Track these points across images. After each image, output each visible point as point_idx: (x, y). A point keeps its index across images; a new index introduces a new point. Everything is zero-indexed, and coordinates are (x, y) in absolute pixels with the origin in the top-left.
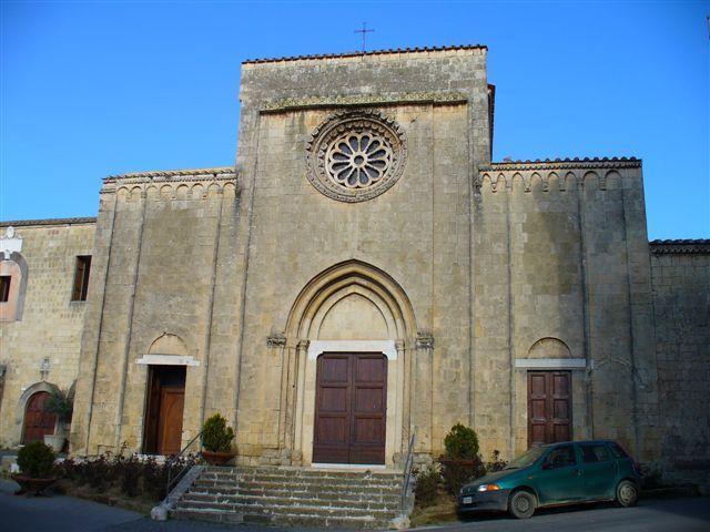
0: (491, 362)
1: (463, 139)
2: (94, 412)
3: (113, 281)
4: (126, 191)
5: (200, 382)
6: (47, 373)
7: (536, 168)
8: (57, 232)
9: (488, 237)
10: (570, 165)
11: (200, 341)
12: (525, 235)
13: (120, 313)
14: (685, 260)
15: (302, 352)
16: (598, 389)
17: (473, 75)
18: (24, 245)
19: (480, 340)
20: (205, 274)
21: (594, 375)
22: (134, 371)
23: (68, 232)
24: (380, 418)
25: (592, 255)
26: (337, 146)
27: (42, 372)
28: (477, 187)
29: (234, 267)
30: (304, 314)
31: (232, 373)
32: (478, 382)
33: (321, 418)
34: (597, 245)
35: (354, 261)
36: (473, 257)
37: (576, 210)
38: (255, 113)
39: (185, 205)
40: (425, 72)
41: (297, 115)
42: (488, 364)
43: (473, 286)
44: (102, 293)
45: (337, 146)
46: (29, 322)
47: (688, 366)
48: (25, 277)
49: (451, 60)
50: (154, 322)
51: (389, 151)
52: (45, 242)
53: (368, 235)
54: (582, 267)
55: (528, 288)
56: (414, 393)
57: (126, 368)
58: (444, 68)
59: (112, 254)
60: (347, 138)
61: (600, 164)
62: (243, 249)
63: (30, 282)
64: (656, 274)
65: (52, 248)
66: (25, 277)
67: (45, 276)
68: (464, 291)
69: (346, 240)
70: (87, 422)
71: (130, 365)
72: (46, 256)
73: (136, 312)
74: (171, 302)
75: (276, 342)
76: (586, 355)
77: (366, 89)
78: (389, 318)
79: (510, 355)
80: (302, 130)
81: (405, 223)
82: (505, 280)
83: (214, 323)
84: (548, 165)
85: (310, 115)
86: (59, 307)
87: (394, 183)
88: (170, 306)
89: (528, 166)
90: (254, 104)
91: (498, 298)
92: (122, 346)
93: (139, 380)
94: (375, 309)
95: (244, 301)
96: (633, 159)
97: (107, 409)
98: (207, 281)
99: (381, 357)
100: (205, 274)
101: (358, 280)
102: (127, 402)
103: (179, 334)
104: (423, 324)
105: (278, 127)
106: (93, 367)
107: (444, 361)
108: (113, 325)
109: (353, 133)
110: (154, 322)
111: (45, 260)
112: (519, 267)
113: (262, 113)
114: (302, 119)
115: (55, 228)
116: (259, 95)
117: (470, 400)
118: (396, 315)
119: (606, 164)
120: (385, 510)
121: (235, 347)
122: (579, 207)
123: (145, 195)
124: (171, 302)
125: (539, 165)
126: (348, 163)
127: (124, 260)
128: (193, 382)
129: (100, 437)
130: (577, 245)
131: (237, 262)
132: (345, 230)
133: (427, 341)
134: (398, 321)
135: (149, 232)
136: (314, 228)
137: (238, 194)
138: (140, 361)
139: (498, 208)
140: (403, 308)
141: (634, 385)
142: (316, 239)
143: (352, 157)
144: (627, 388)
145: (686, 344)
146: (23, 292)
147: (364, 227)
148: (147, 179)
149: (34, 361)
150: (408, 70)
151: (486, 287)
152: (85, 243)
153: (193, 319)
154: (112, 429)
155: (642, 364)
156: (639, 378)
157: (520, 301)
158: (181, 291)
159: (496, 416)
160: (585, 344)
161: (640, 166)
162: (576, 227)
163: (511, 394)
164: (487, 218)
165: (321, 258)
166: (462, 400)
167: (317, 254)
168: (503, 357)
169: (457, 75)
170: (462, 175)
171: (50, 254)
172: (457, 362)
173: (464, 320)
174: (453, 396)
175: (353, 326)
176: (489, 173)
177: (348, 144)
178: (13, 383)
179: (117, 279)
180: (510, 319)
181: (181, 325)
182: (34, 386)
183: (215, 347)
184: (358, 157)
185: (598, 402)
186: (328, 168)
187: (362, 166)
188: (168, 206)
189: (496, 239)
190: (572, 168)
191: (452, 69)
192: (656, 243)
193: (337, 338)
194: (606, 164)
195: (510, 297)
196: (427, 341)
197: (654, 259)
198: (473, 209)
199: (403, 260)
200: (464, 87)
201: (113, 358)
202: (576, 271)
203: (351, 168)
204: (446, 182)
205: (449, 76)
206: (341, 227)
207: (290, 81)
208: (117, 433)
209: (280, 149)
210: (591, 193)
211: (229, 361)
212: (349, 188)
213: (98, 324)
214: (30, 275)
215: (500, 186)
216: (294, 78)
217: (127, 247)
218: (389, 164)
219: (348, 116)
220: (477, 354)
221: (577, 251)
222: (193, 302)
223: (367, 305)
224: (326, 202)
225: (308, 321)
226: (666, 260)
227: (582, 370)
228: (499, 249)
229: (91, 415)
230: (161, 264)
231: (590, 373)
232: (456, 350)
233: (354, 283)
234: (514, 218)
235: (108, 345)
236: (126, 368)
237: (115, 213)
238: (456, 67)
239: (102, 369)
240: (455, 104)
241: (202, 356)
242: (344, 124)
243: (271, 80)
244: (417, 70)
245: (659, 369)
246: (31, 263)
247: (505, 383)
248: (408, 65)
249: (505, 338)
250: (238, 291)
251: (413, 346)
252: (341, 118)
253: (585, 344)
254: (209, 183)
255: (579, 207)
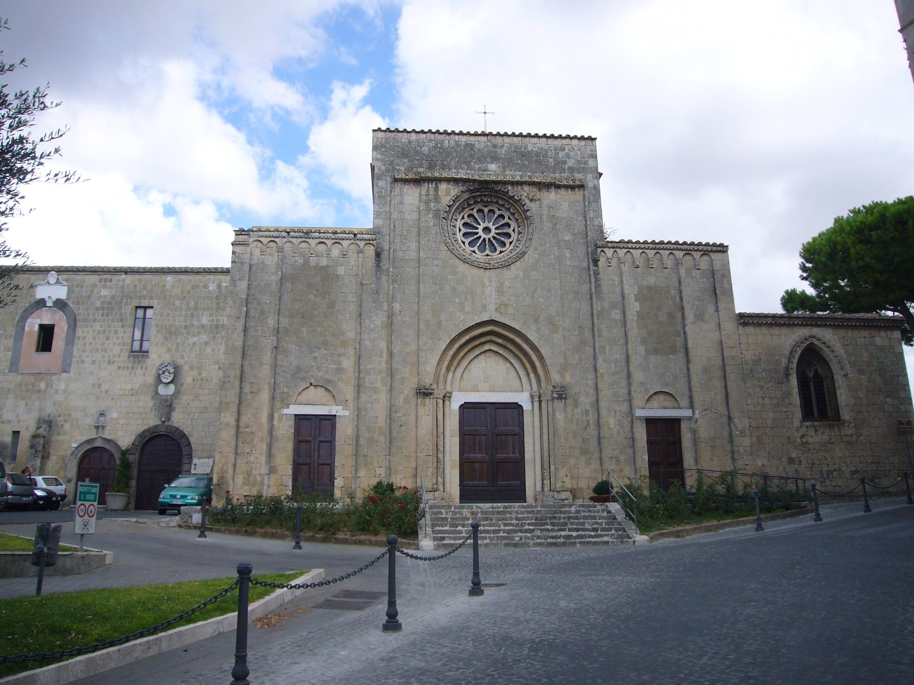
0: (615, 412)
1: (581, 218)
2: (238, 461)
3: (252, 333)
4: (259, 244)
5: (350, 431)
6: (103, 427)
7: (644, 248)
8: (111, 281)
9: (606, 305)
10: (672, 247)
11: (350, 395)
12: (637, 304)
13: (261, 364)
14: (764, 330)
15: (447, 402)
16: (703, 434)
17: (586, 163)
18: (70, 292)
19: (606, 393)
20: (349, 329)
21: (699, 423)
22: (280, 419)
23: (124, 281)
24: (520, 463)
25: (692, 323)
26: (466, 216)
27: (97, 427)
28: (596, 262)
29: (378, 323)
30: (448, 369)
31: (382, 421)
32: (606, 429)
33: (465, 466)
34: (695, 315)
35: (492, 322)
36: (596, 321)
37: (677, 285)
38: (389, 179)
39: (324, 262)
40: (545, 156)
41: (432, 186)
42: (613, 413)
43: (597, 346)
44: (240, 343)
45: (466, 216)
46: (80, 374)
47: (772, 416)
48: (73, 324)
49: (567, 148)
50: (298, 373)
51: (513, 224)
52: (96, 290)
53: (505, 299)
54: (685, 333)
55: (641, 349)
56: (552, 440)
57: (271, 418)
58: (561, 154)
59: (250, 306)
60: (475, 210)
61: (696, 248)
62: (385, 308)
63: (79, 332)
64: (743, 341)
65: (105, 296)
66: (73, 324)
67: (97, 327)
68: (589, 350)
69: (484, 302)
70: (230, 472)
71: (276, 415)
72: (98, 304)
73: (279, 363)
74: (316, 355)
75: (424, 393)
76: (692, 406)
77: (493, 167)
78: (522, 373)
79: (631, 405)
80: (437, 199)
81: (536, 290)
82: (623, 342)
83: (362, 375)
84: (654, 246)
85: (443, 186)
86: (116, 359)
87: (524, 253)
88: (315, 358)
89: (638, 246)
90: (388, 171)
91: (618, 357)
92: (265, 396)
93: (285, 430)
94: (508, 365)
95: (391, 355)
96: (721, 245)
97: (252, 459)
98: (351, 335)
99: (517, 407)
100: (349, 329)
101: (494, 338)
102: (275, 451)
103: (326, 386)
104: (556, 378)
105: (411, 196)
106: (235, 416)
107: (575, 410)
108: (255, 376)
109: (480, 206)
110: (298, 373)
111: (97, 309)
112: (634, 331)
113: (396, 180)
114: (436, 189)
115: (109, 277)
116: (391, 164)
117: (599, 444)
118: (530, 370)
119: (701, 248)
120: (613, 532)
121: (383, 398)
122: (680, 282)
123: (280, 250)
124: (316, 355)
125: (647, 246)
126: (477, 233)
127: (263, 312)
128: (344, 432)
129: (246, 488)
130: (679, 314)
131: (378, 319)
132: (483, 293)
133: (561, 394)
134: (532, 375)
135: (288, 285)
136: (454, 289)
137: (378, 255)
138: (286, 411)
139: (613, 281)
140: (537, 364)
141: (731, 430)
142: (457, 300)
143: (481, 228)
144: (726, 434)
145: (769, 397)
146: (71, 339)
147: (500, 291)
148: (284, 234)
149: (86, 416)
150: (529, 153)
151: (607, 347)
152: (145, 293)
153: (340, 370)
154: (259, 478)
155: (735, 414)
156: (735, 425)
157: (636, 360)
158: (325, 343)
159: (622, 458)
160: (691, 397)
161: (726, 251)
162: (678, 299)
163: (633, 439)
164: (605, 288)
165: (462, 317)
166: (593, 443)
167: (459, 314)
168: (624, 407)
169: (572, 161)
170: (581, 251)
171: (103, 303)
172: (587, 412)
173: (591, 376)
174: (584, 441)
175: (490, 381)
176: (605, 250)
177: (476, 216)
178: (59, 437)
179: (256, 331)
180: (629, 375)
181: (327, 376)
182: (88, 442)
183: (364, 397)
184: (487, 227)
185: (703, 445)
186: (459, 236)
187: (487, 237)
188: (306, 262)
189: (614, 306)
190: (674, 249)
191: (568, 156)
192: (742, 316)
193: (475, 389)
194: (701, 248)
195: (628, 356)
196: (561, 394)
197: (741, 328)
198: (593, 280)
199: (536, 321)
200: (579, 173)
201: (257, 409)
202: (680, 336)
203: (480, 237)
204: (568, 255)
205: (565, 162)
206: (479, 290)
207: (421, 153)
208: (266, 482)
209: (415, 216)
210: (688, 271)
211: (378, 410)
212: (479, 256)
213: (238, 373)
214: (78, 324)
215: (614, 262)
216: (425, 150)
217: (265, 299)
218: (514, 236)
219: (478, 190)
220: (603, 404)
221: (679, 320)
222: (340, 355)
223: (501, 362)
224: (463, 268)
225: (451, 374)
226: (750, 330)
227: (690, 419)
228: (616, 315)
229: (235, 465)
230: (303, 317)
231: (696, 421)
232: (586, 401)
233: (491, 341)
234: (627, 290)
235: (250, 396)
236: (271, 418)
237: (251, 266)
238: (572, 154)
239: (244, 420)
240: (573, 188)
241: (351, 404)
242: (474, 197)
243: (403, 149)
244: (538, 154)
245: (749, 418)
246: (80, 311)
247: (628, 429)
248: (530, 148)
249: (625, 391)
250: (383, 345)
251: (549, 397)
252: (472, 191)
253: (691, 397)
254: (349, 242)
255: (680, 282)
